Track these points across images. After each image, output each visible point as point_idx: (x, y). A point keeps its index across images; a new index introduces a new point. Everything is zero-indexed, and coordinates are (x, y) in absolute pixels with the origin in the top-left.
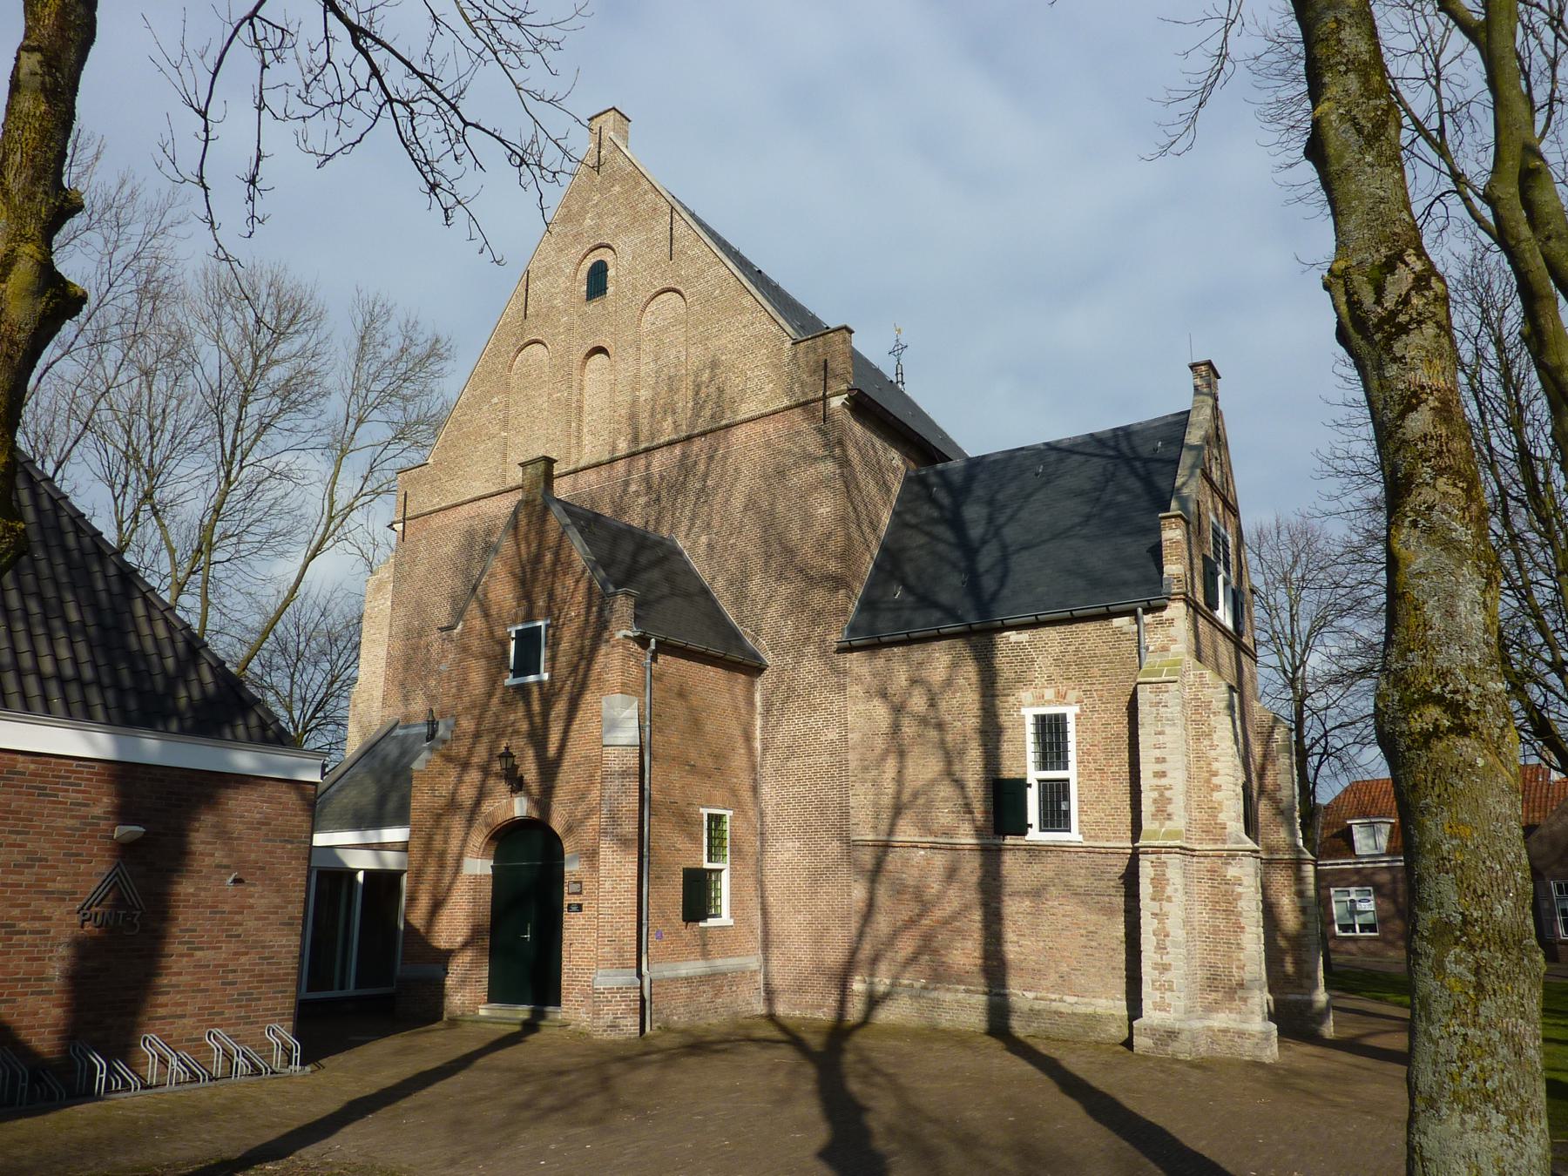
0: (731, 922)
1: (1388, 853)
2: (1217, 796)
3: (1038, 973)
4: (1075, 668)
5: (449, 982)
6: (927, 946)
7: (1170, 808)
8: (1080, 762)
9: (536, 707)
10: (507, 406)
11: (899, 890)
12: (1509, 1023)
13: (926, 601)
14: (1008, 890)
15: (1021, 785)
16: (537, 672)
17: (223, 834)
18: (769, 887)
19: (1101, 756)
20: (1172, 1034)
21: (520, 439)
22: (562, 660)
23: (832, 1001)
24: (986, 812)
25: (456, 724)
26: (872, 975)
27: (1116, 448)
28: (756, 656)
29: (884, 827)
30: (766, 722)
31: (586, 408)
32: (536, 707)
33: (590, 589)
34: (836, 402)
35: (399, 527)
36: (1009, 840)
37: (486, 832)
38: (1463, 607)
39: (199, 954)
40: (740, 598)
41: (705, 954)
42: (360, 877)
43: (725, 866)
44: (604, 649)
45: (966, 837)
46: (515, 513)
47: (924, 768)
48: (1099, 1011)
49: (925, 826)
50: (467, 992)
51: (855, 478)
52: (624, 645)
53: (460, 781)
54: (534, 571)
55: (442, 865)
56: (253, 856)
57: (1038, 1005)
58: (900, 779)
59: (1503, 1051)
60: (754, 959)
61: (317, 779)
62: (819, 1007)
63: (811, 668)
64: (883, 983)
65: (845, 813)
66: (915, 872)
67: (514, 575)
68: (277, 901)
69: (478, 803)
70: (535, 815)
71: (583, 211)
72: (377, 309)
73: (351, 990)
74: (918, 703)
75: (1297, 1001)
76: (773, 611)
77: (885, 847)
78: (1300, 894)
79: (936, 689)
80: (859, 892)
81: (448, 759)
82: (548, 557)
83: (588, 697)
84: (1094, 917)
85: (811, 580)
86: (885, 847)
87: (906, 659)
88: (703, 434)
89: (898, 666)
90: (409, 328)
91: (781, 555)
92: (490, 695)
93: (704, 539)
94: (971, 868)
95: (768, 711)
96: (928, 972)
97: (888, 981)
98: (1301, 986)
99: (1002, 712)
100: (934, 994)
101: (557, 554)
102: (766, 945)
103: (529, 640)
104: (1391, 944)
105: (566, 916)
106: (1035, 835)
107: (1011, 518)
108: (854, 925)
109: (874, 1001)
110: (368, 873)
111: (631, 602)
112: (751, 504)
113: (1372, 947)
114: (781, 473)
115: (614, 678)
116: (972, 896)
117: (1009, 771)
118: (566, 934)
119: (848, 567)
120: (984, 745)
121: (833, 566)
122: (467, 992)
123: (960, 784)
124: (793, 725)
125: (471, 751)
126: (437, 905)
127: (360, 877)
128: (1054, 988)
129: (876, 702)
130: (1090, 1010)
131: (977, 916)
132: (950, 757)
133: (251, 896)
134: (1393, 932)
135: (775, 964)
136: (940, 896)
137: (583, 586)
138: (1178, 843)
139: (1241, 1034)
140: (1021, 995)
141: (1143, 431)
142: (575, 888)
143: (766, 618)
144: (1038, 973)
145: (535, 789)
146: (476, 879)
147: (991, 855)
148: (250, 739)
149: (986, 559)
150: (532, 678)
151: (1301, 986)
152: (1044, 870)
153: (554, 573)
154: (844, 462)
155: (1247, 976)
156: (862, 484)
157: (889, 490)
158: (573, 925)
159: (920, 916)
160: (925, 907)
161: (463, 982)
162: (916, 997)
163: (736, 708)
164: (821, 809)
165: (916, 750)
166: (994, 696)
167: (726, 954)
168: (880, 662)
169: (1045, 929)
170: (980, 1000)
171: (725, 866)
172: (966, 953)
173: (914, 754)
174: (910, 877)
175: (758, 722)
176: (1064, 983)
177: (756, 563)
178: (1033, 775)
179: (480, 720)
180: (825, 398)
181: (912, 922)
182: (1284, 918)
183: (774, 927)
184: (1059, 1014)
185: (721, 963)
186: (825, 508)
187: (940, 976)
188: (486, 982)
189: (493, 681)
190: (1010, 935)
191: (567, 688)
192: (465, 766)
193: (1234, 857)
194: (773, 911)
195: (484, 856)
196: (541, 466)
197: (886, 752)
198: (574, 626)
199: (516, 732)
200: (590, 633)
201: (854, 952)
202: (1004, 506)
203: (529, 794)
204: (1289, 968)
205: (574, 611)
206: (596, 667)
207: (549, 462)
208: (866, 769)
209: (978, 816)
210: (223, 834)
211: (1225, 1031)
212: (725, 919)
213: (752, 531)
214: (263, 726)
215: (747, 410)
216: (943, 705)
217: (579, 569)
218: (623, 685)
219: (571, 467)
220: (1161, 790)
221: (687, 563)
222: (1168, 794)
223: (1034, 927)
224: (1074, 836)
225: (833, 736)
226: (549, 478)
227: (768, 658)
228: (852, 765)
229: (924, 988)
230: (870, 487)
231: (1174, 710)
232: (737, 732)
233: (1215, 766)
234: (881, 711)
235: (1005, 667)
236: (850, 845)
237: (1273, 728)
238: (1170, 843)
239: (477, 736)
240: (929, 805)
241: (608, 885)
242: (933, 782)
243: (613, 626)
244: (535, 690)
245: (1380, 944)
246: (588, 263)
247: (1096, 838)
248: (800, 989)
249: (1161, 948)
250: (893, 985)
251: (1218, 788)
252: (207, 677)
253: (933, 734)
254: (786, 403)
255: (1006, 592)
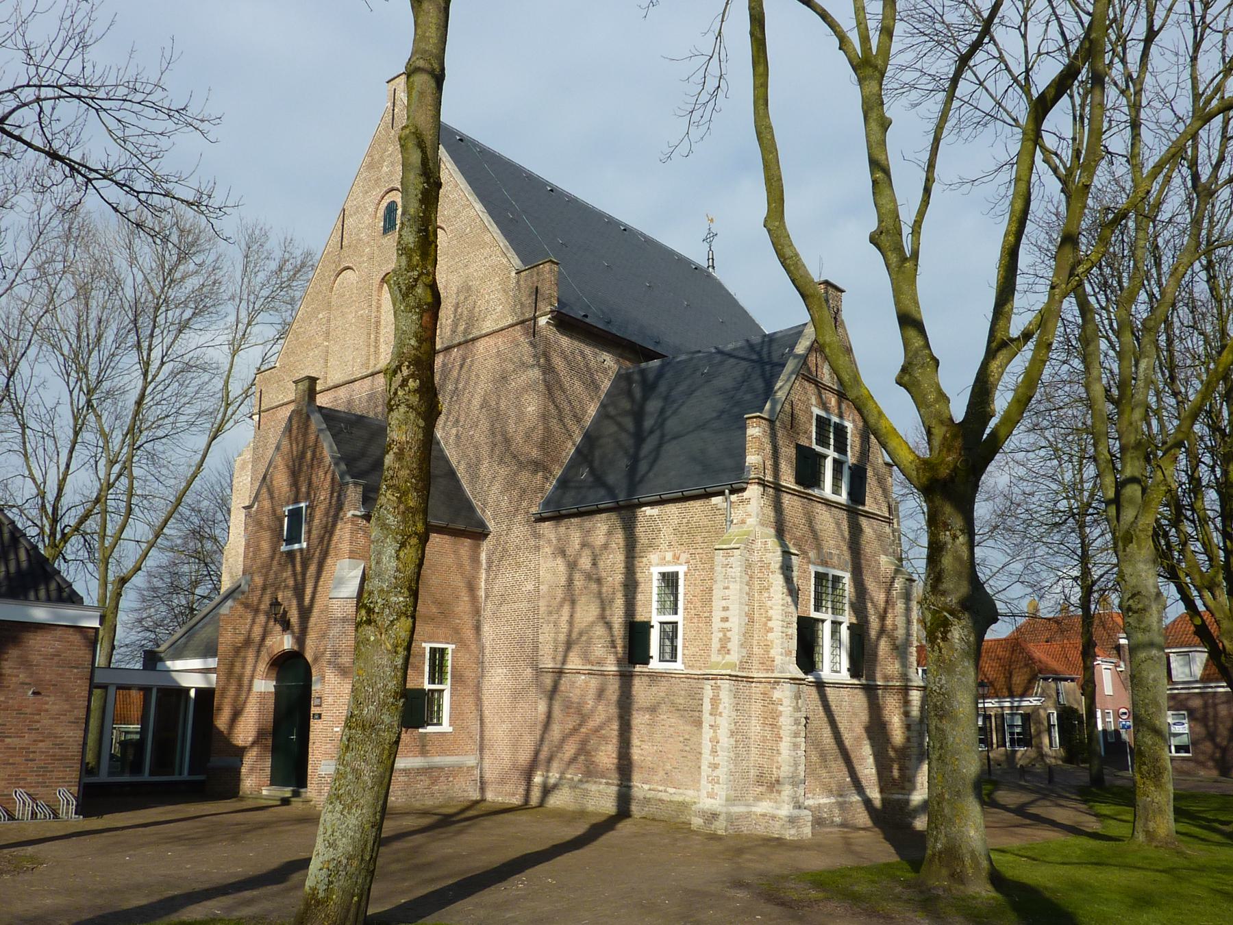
0: (450, 729)
1: (1202, 680)
2: (770, 636)
3: (652, 770)
4: (687, 536)
5: (243, 770)
6: (583, 749)
7: (729, 646)
8: (685, 609)
9: (299, 568)
10: (329, 321)
11: (568, 705)
12: (356, 764)
13: (599, 480)
14: (636, 706)
15: (647, 626)
16: (300, 542)
17: (25, 663)
18: (486, 703)
19: (699, 605)
20: (715, 816)
21: (336, 348)
22: (315, 533)
23: (521, 790)
24: (624, 647)
25: (252, 579)
26: (548, 771)
27: (759, 353)
28: (482, 525)
29: (559, 658)
30: (488, 576)
31: (382, 322)
32: (299, 568)
33: (333, 479)
34: (543, 321)
35: (256, 417)
36: (638, 668)
37: (267, 659)
38: (385, 559)
39: (8, 740)
40: (474, 477)
41: (424, 752)
42: (192, 693)
43: (447, 687)
44: (339, 525)
45: (611, 667)
46: (290, 419)
47: (587, 612)
48: (687, 799)
49: (586, 658)
50: (255, 778)
51: (559, 382)
52: (352, 522)
53: (253, 622)
54: (300, 465)
55: (240, 686)
56: (48, 677)
57: (650, 795)
58: (571, 623)
59: (350, 777)
60: (472, 757)
61: (97, 625)
62: (514, 795)
63: (520, 531)
64: (554, 777)
65: (536, 648)
66: (578, 692)
67: (288, 466)
68: (66, 707)
69: (263, 639)
70: (296, 648)
71: (382, 159)
72: (257, 232)
73: (185, 776)
74: (585, 562)
75: (899, 800)
76: (496, 488)
77: (560, 673)
78: (907, 714)
79: (598, 552)
80: (542, 707)
81: (246, 606)
82: (309, 454)
83: (329, 561)
84: (688, 728)
85: (522, 465)
86: (560, 673)
87: (581, 527)
88: (459, 344)
89: (573, 532)
90: (288, 243)
91: (503, 445)
92: (272, 558)
93: (454, 431)
94: (613, 687)
95: (489, 567)
96: (584, 769)
97: (558, 776)
98: (903, 788)
99: (638, 570)
100: (585, 786)
101: (314, 453)
102: (481, 750)
103: (295, 515)
104: (1202, 764)
105: (312, 722)
106: (655, 664)
107: (674, 413)
108: (538, 732)
109: (547, 791)
110: (198, 690)
111: (360, 489)
112: (484, 404)
113: (1185, 766)
114: (504, 378)
115: (345, 547)
116: (613, 711)
117: (640, 617)
118: (311, 736)
119: (548, 454)
120: (626, 595)
121: (535, 453)
122: (255, 778)
123: (609, 626)
124: (506, 578)
125: (260, 601)
126: (236, 714)
127: (192, 693)
128: (663, 782)
129: (560, 561)
130: (680, 799)
131: (615, 726)
132: (604, 605)
133: (47, 703)
134: (1204, 753)
135: (487, 763)
136: (593, 711)
137: (329, 477)
138: (729, 672)
139: (773, 817)
140: (641, 787)
141: (783, 337)
142: (317, 702)
143: (490, 491)
144: (652, 770)
145: (296, 629)
146: (262, 695)
147: (626, 678)
148: (49, 599)
149: (647, 447)
150: (296, 546)
151: (903, 788)
152: (660, 690)
153: (312, 466)
154: (548, 369)
155: (782, 775)
156: (567, 385)
157: (597, 388)
158: (316, 726)
159: (580, 725)
160: (584, 719)
161: (252, 770)
162: (573, 787)
163: (460, 566)
164: (521, 643)
165: (583, 599)
166: (634, 557)
167: (443, 752)
168: (562, 529)
169: (658, 737)
170: (613, 790)
171: (447, 687)
172: (607, 756)
173: (582, 601)
174: (575, 696)
175: (483, 576)
176: (668, 780)
177: (485, 451)
178: (656, 619)
179: (266, 575)
180: (535, 318)
181: (575, 730)
182: (894, 733)
183: (487, 734)
184: (661, 801)
185: (438, 760)
186: (532, 406)
187: (591, 772)
188: (268, 771)
189: (274, 549)
190: (635, 741)
191: (317, 554)
192: (257, 611)
193: (778, 683)
194: (487, 721)
195: (267, 677)
196: (306, 383)
197: (564, 600)
198: (323, 507)
199: (286, 587)
200: (332, 513)
201: (537, 753)
202: (673, 402)
203: (293, 633)
204: (896, 773)
205: (323, 495)
206: (335, 538)
207: (313, 380)
208: (550, 613)
209: (620, 649)
210: (25, 663)
211: (764, 815)
212: (446, 727)
213: (484, 425)
214: (60, 589)
215: (488, 325)
216: (601, 564)
217: (327, 464)
218: (351, 552)
219: (369, 372)
220: (725, 631)
221: (442, 451)
222: (729, 634)
223: (651, 734)
224: (678, 666)
225: (530, 587)
226: (312, 393)
227: (491, 525)
228: (542, 609)
229: (580, 781)
230: (576, 387)
231: (736, 570)
232: (459, 582)
233: (771, 612)
234: (561, 566)
235: (642, 535)
236: (539, 672)
237: (893, 578)
238: (724, 672)
239: (264, 588)
240: (589, 642)
241: (330, 700)
242: (592, 624)
243: (346, 507)
244: (298, 554)
245: (1192, 764)
246: (384, 204)
247: (692, 667)
248: (502, 781)
249: (714, 752)
250: (561, 778)
251: (771, 630)
252: (23, 556)
253: (594, 586)
254: (510, 322)
255: (651, 475)
